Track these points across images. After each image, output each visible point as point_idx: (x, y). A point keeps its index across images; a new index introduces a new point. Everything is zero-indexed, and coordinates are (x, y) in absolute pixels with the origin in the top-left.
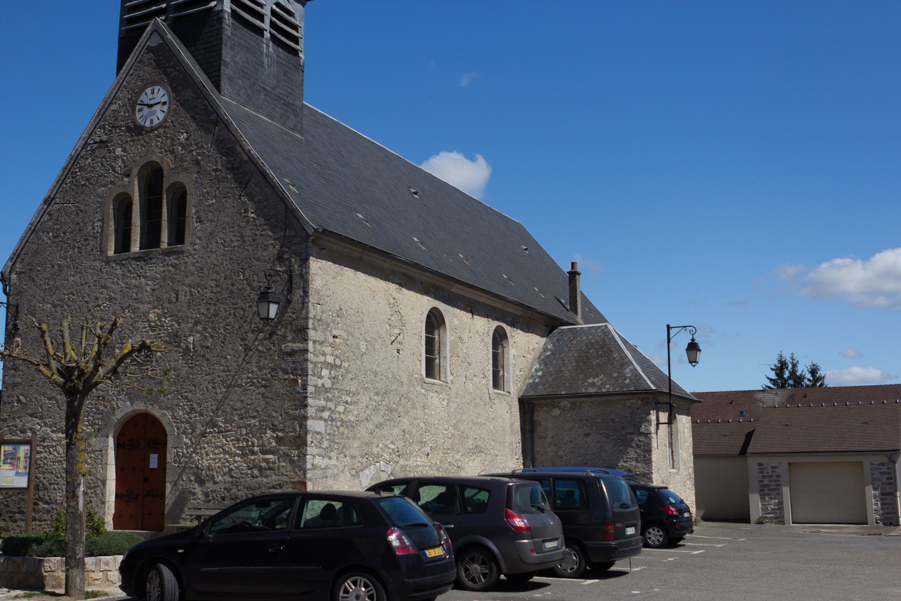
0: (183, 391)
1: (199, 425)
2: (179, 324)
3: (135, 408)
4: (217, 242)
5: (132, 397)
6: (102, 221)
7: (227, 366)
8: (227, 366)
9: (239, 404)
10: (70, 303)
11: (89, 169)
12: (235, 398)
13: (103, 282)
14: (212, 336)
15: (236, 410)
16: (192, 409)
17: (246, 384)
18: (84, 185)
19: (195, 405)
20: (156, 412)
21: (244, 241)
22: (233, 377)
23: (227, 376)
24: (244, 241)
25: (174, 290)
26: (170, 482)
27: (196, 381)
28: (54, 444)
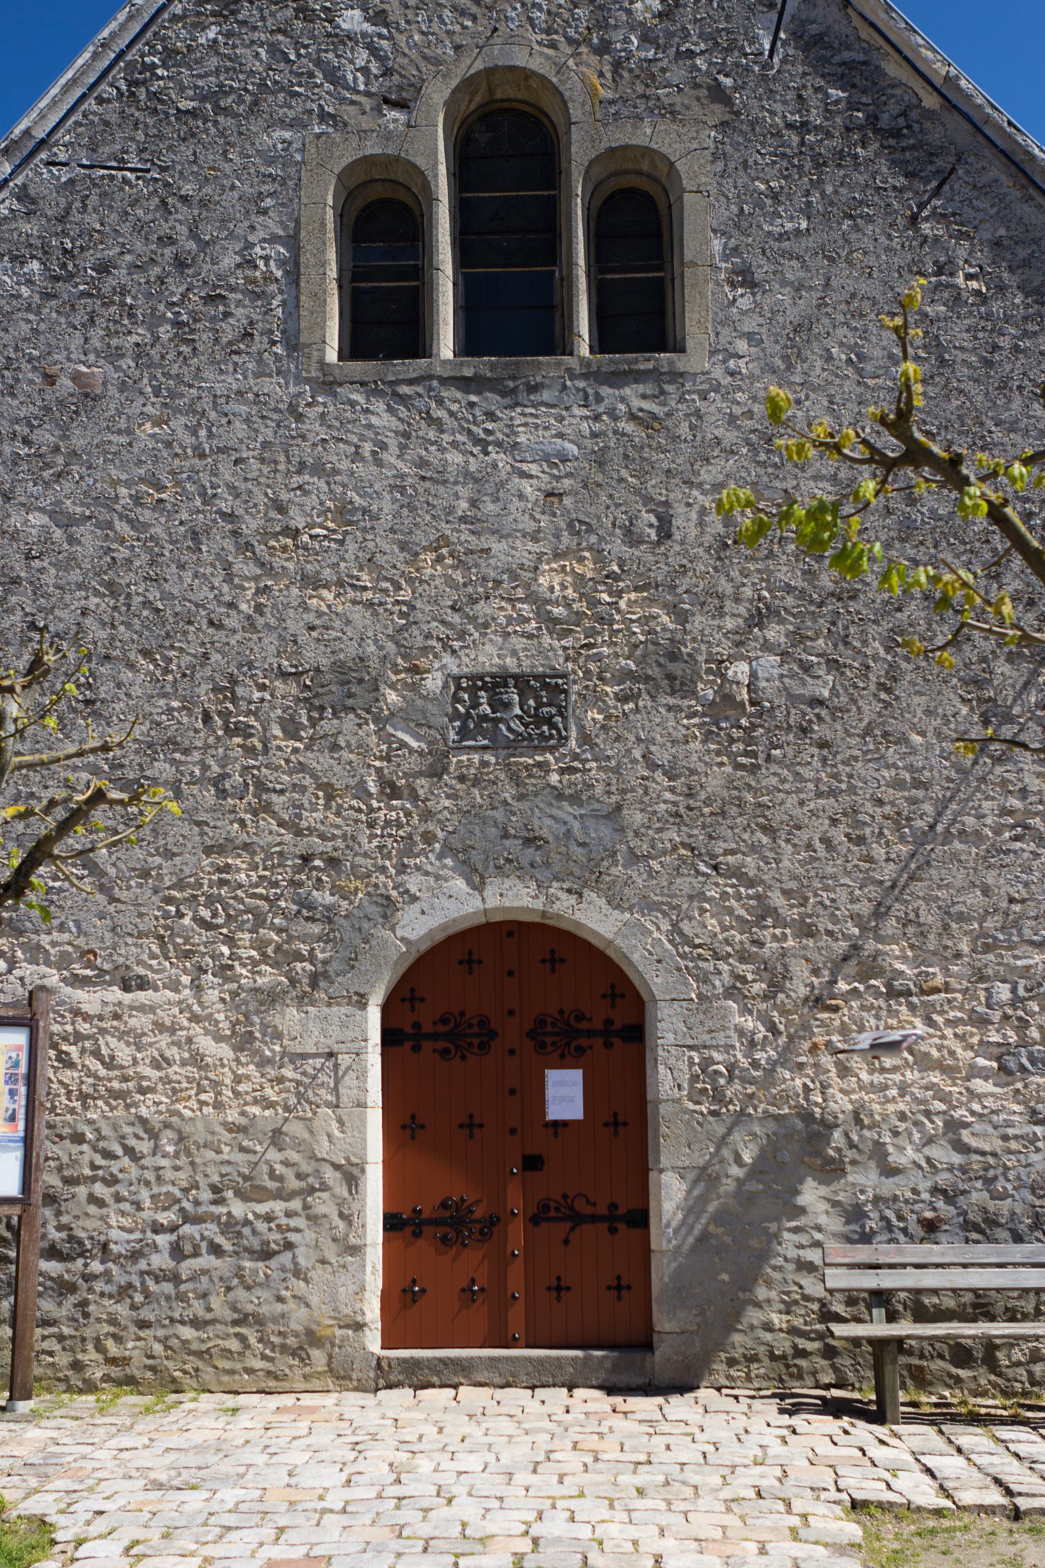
0: (719, 847)
1: (800, 970)
2: (683, 617)
3: (493, 901)
4: (829, 358)
5: (476, 858)
6: (293, 241)
7: (911, 768)
8: (911, 768)
9: (975, 899)
10: (146, 515)
11: (213, 62)
12: (959, 877)
13: (304, 451)
14: (834, 665)
15: (961, 918)
16: (765, 912)
17: (998, 831)
18: (192, 113)
19: (777, 899)
20: (597, 919)
21: (942, 362)
22: (941, 806)
23: (914, 801)
24: (942, 362)
25: (648, 500)
26: (682, 1172)
27: (777, 817)
28: (84, 1027)
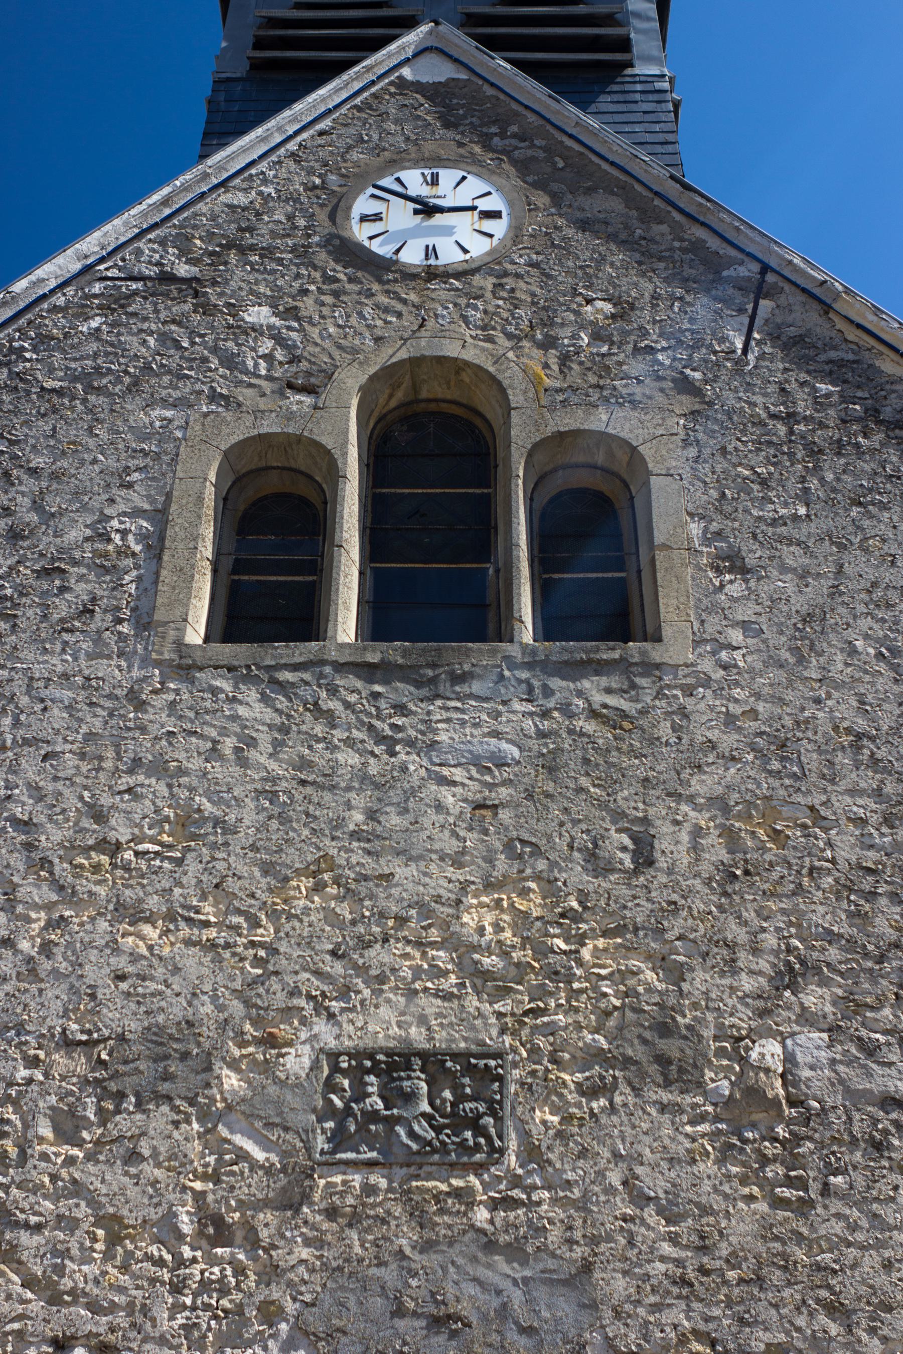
27: (850, 1289)
